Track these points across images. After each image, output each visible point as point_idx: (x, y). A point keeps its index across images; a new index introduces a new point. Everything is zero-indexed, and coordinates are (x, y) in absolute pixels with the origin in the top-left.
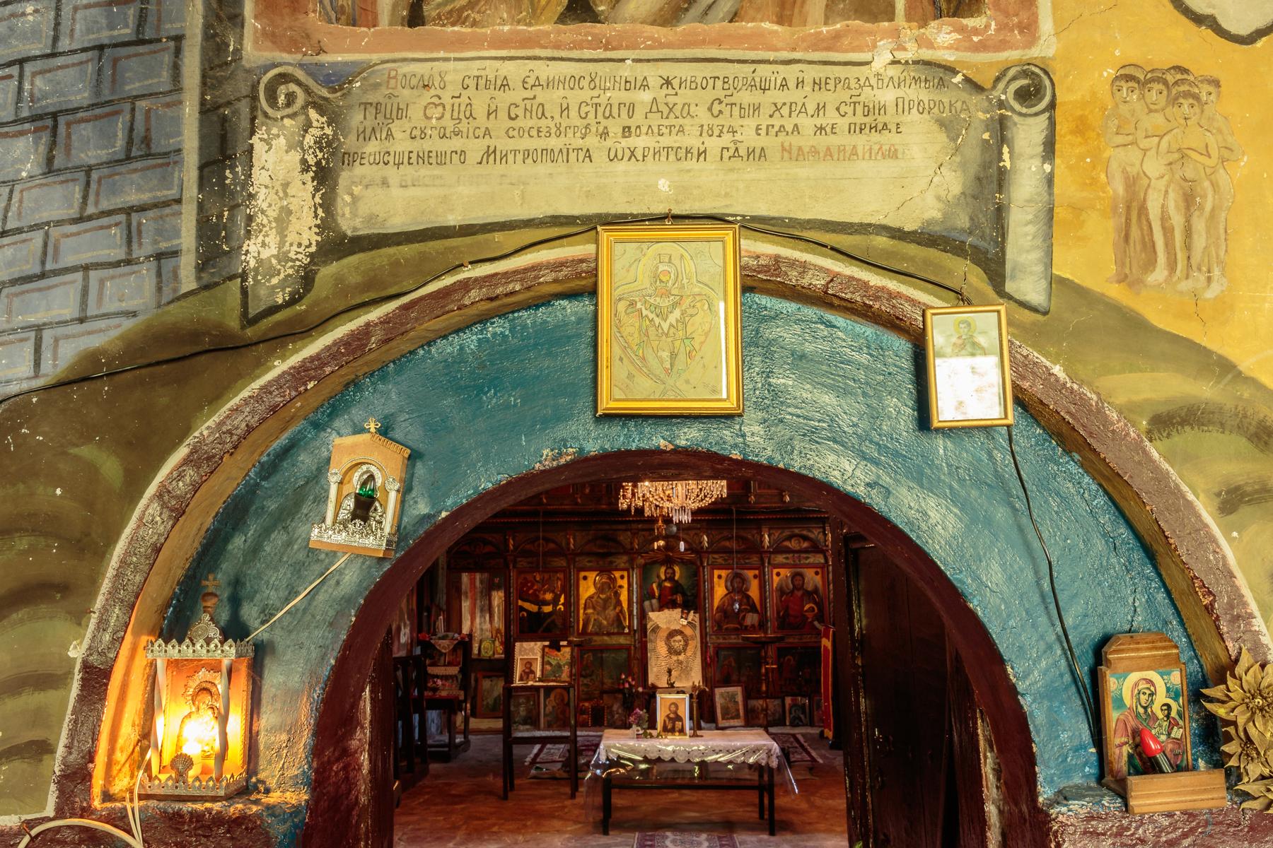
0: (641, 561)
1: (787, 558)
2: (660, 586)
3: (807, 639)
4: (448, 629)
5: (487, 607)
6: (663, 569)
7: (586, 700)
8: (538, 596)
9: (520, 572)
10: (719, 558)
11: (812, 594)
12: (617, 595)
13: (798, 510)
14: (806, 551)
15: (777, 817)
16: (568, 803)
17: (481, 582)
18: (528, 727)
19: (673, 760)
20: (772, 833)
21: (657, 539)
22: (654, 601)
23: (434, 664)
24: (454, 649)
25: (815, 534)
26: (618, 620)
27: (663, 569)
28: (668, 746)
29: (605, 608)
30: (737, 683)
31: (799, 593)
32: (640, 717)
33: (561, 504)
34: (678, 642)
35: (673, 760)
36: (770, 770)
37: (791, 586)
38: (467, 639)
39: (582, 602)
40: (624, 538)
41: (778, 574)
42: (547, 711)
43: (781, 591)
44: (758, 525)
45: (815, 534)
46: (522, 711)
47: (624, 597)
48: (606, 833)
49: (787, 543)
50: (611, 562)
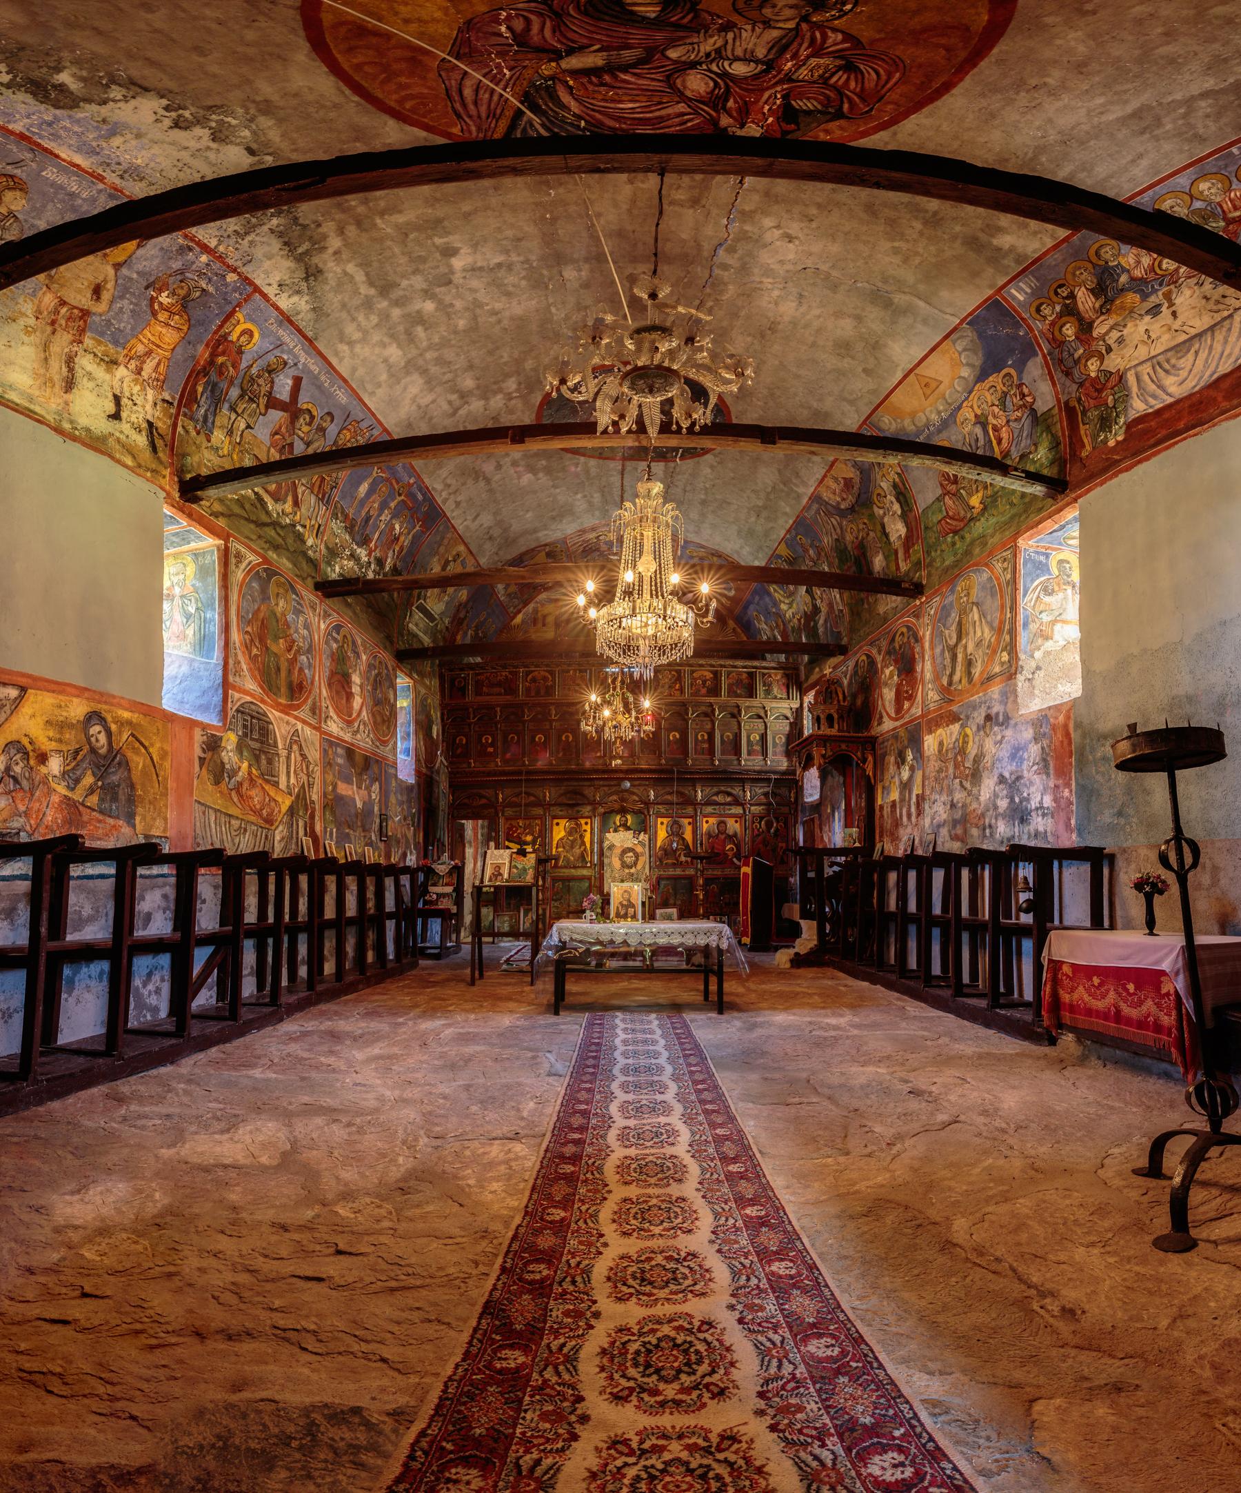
0: (601, 810)
3: (729, 871)
10: (662, 809)
11: (732, 838)
12: (582, 837)
13: (725, 772)
14: (729, 804)
15: (726, 999)
16: (527, 989)
19: (625, 942)
20: (721, 1012)
21: (615, 758)
23: (434, 885)
24: (450, 873)
25: (737, 791)
26: (582, 857)
28: (623, 930)
29: (572, 847)
30: (674, 906)
32: (593, 902)
34: (629, 857)
35: (625, 942)
36: (720, 951)
40: (588, 792)
43: (709, 835)
44: (693, 782)
45: (737, 791)
47: (587, 839)
48: (557, 1013)
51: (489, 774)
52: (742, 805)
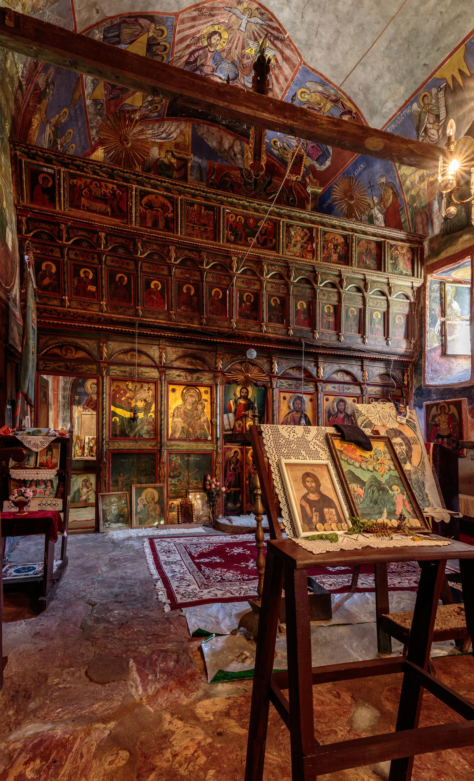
1: (334, 387)
2: (236, 402)
4: (36, 423)
5: (68, 418)
6: (239, 388)
7: (175, 498)
8: (130, 403)
9: (113, 380)
17: (64, 398)
18: (120, 525)
22: (231, 415)
27: (239, 388)
31: (342, 416)
33: (157, 318)
37: (336, 410)
38: (67, 436)
39: (171, 411)
41: (327, 400)
42: (139, 510)
45: (355, 369)
46: (114, 509)
49: (334, 376)
50: (198, 378)
51: (90, 320)
52: (360, 385)
